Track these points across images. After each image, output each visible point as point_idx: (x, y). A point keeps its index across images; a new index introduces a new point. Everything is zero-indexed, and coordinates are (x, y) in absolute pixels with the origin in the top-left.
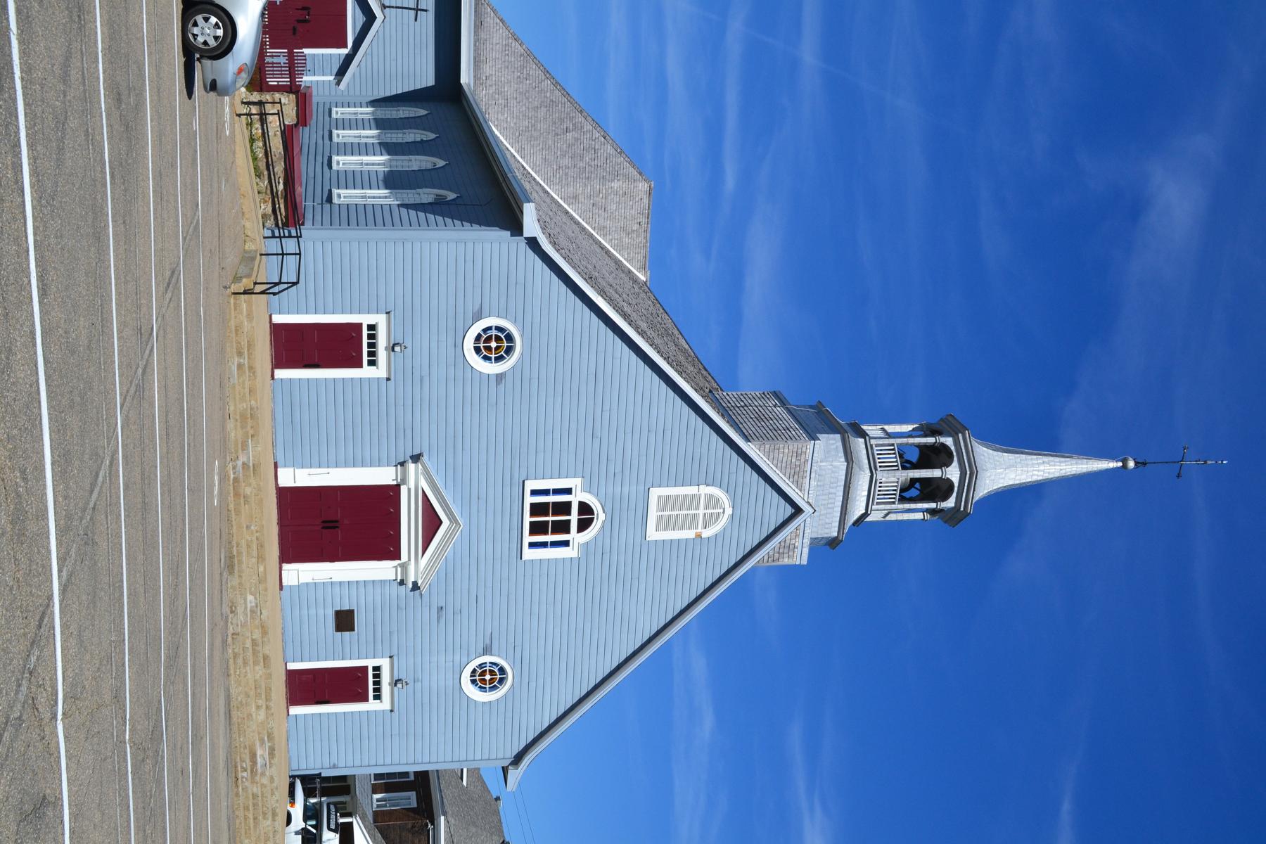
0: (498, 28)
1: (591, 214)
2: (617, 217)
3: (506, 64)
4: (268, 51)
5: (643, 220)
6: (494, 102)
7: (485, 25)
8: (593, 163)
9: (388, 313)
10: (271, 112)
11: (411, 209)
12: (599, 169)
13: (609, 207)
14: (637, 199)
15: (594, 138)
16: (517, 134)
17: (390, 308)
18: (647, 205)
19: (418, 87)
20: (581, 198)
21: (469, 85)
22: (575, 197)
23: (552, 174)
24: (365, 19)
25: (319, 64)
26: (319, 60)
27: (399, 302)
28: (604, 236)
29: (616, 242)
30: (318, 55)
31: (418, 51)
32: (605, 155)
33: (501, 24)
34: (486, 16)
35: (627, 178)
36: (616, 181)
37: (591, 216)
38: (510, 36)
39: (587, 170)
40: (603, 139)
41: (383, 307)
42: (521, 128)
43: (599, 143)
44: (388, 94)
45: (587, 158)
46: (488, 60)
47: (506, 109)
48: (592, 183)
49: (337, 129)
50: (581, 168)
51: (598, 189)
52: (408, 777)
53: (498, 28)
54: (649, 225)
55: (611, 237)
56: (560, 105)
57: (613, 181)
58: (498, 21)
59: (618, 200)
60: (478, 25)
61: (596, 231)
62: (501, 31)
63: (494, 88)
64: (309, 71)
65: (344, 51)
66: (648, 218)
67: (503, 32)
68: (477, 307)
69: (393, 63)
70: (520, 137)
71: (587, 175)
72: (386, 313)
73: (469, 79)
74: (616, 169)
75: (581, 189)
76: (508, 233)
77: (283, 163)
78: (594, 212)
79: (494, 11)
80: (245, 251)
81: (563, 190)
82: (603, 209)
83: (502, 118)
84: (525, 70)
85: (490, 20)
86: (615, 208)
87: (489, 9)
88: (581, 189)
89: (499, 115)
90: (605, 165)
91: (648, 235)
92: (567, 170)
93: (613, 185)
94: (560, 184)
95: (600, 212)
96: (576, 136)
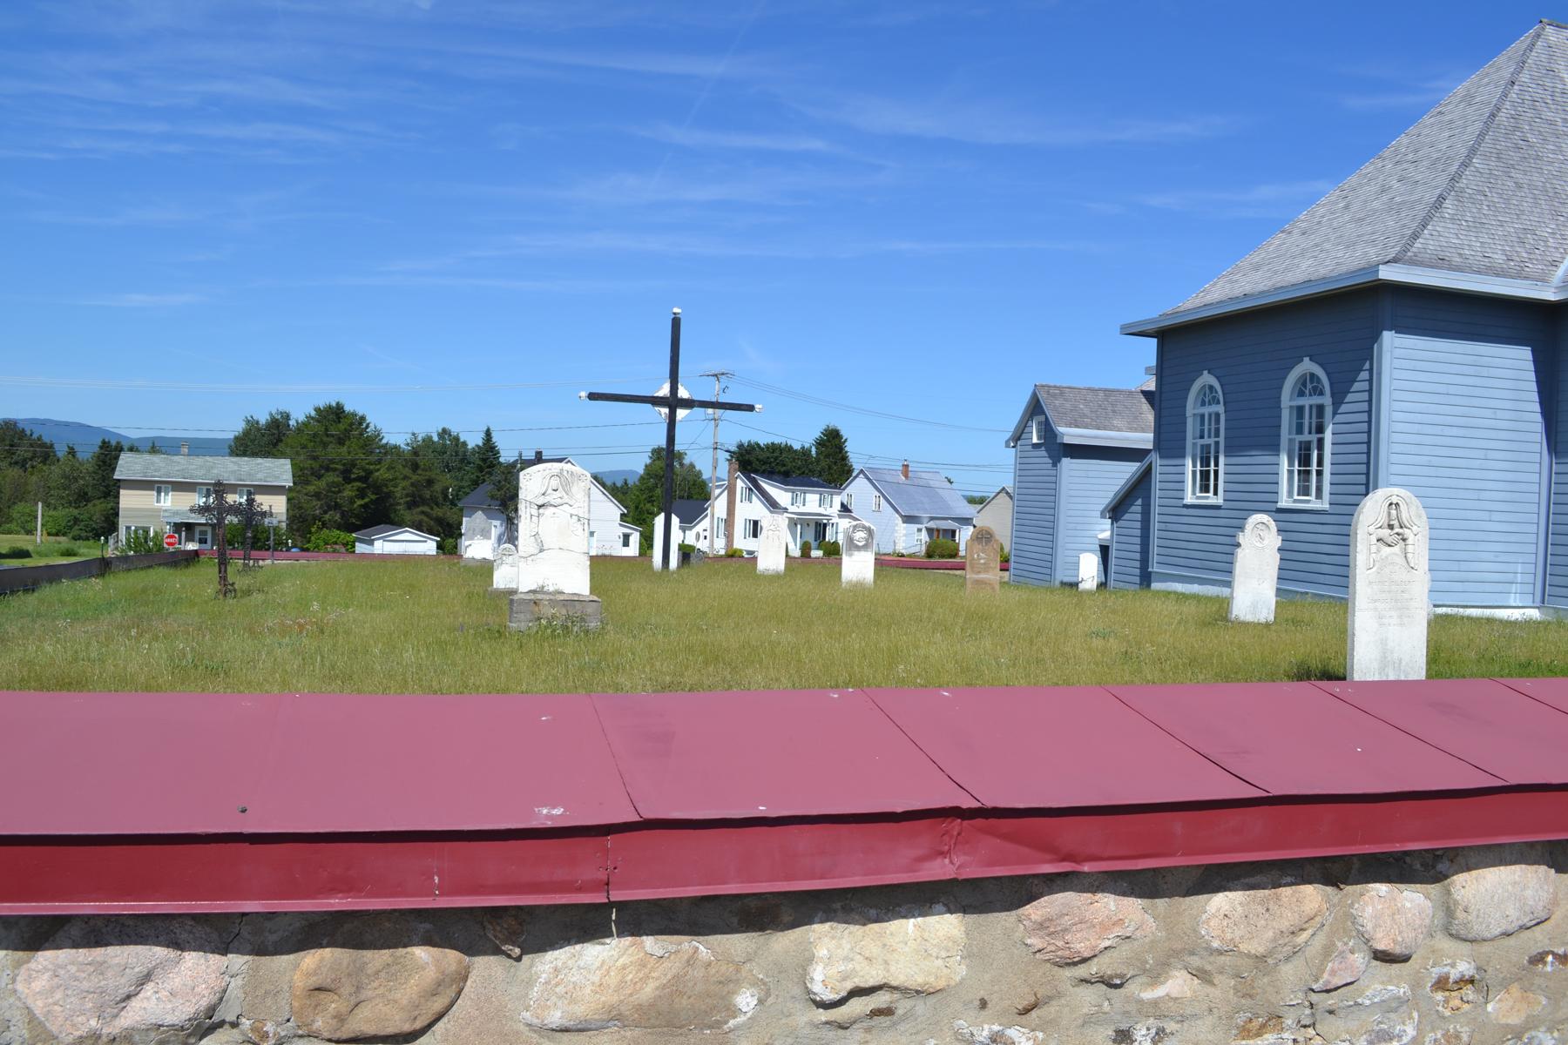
8: (1552, 106)
15: (1519, 101)
16: (1562, 219)
33: (1429, 227)
36: (1561, 75)
39: (1563, 116)
40: (1516, 87)
42: (1554, 212)
45: (1548, 114)
58: (1426, 232)
60: (1440, 263)
79: (1415, 236)
83: (1551, 240)
90: (1547, 88)
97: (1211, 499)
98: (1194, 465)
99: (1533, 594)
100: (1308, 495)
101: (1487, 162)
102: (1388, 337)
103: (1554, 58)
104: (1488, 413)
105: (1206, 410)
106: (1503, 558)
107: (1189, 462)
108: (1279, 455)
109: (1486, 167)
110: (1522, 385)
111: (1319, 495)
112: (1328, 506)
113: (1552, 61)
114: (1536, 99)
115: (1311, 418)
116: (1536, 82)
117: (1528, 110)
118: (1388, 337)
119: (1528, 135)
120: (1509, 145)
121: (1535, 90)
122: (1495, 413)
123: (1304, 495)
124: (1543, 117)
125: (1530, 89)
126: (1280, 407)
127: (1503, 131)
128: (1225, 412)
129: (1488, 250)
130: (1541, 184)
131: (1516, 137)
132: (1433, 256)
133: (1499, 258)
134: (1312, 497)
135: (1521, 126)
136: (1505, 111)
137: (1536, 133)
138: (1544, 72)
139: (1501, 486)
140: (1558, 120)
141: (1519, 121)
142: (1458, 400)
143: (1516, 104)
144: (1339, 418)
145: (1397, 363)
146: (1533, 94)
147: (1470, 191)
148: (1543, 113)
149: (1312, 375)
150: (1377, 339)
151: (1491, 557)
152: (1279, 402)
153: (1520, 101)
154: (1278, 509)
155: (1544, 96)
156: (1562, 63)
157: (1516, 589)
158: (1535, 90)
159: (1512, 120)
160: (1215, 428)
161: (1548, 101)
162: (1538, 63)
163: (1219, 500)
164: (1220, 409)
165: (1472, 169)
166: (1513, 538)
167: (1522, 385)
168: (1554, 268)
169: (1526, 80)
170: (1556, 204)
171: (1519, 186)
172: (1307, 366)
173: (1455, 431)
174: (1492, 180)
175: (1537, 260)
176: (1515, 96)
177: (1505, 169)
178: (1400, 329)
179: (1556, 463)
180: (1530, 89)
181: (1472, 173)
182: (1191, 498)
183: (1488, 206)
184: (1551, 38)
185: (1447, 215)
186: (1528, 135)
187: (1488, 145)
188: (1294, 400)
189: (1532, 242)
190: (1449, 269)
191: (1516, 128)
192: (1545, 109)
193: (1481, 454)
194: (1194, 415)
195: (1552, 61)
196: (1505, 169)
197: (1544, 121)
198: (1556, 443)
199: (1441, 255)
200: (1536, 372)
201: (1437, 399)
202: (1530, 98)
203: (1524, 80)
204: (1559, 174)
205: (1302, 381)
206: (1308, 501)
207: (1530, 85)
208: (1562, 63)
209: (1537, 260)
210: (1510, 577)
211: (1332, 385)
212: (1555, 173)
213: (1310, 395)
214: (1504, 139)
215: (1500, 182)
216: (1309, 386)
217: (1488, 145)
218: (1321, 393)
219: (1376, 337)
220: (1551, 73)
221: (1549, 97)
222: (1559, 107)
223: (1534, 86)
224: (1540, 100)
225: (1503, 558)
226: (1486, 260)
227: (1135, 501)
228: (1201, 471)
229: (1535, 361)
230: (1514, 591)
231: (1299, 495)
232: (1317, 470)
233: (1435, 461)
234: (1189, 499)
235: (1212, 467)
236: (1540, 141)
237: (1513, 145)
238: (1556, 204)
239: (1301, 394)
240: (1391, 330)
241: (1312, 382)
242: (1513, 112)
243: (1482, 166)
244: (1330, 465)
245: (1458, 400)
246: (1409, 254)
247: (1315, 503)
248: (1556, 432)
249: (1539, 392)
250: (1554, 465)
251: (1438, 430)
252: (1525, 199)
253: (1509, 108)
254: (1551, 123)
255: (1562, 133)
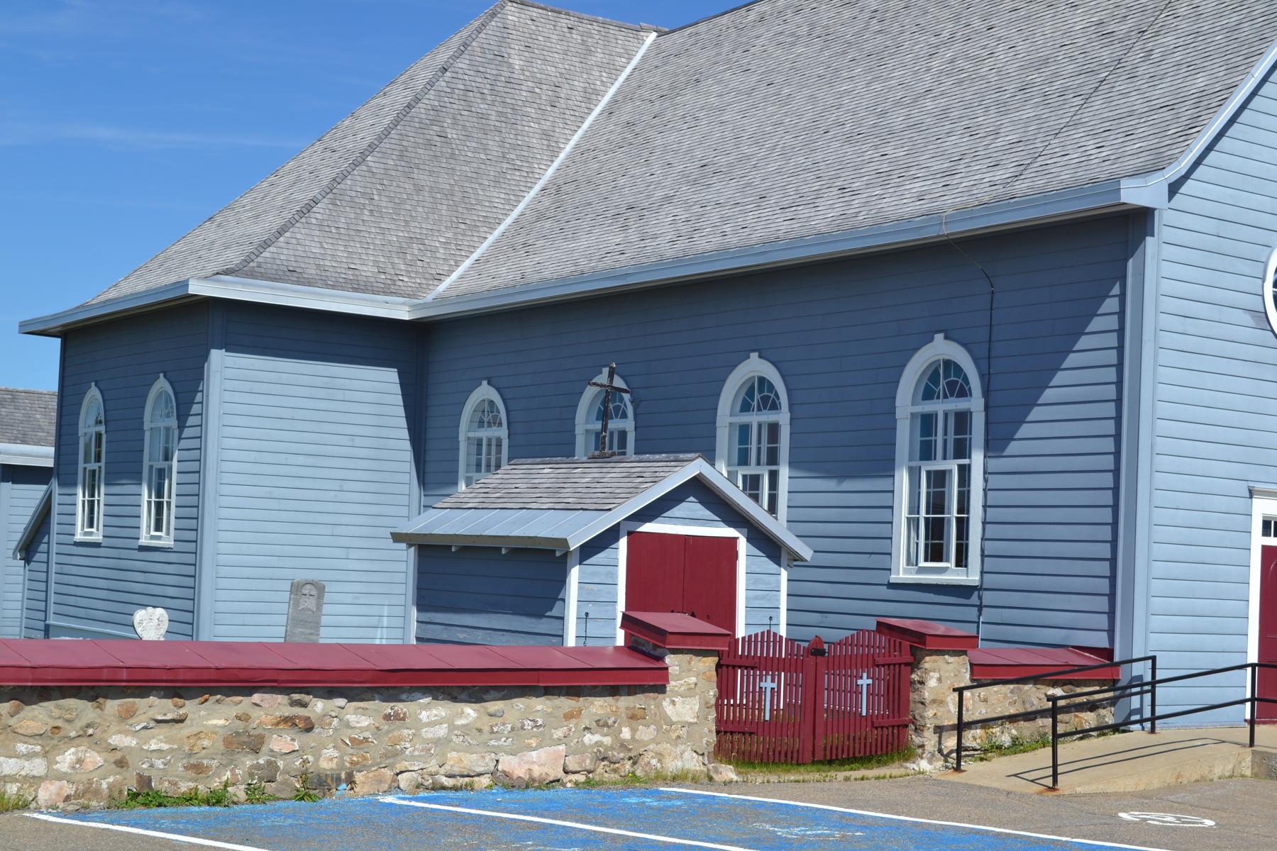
0: (294, 241)
1: (567, 112)
2: (567, 67)
3: (352, 233)
4: (738, 702)
5: (564, 22)
6: (419, 263)
7: (294, 264)
8: (489, 98)
9: (1252, 493)
10: (954, 709)
11: (186, 422)
12: (496, 88)
13: (554, 79)
14: (534, 28)
15: (449, 90)
16: (463, 226)
17: (1242, 489)
18: (540, 11)
19: (399, 400)
20: (546, 125)
21: (415, 307)
22: (546, 135)
23: (518, 173)
24: (692, 499)
25: (763, 598)
26: (756, 598)
27: (1236, 470)
28: (599, 94)
29: (604, 74)
30: (747, 599)
31: (339, 395)
32: (472, 73)
33: (287, 234)
34: (278, 262)
35: (503, 39)
36: (511, 60)
37: (572, 113)
38: (303, 220)
39: (500, 109)
40: (448, 74)
41: (1240, 504)
42: (455, 220)
43: (454, 81)
44: (408, 455)
45: (482, 106)
46: (353, 266)
47: (426, 242)
48: (520, 103)
49: (74, 535)
50: (498, 119)
51: (528, 94)
52: (165, 469)
53: (294, 241)
54: (571, 13)
55: (598, 83)
56: (405, 143)
57: (510, 66)
58: (282, 239)
59: (539, 62)
60: (291, 275)
61: (592, 106)
62: (298, 236)
63: (396, 261)
64: (771, 618)
65: (743, 546)
66: (559, 13)
67: (299, 232)
68: (1247, 319)
69: (358, 441)
70: (468, 222)
71: (509, 111)
72: (1251, 497)
73: (404, 304)
74: (492, 57)
75: (532, 124)
76: (1148, 239)
77: (1026, 687)
78: (564, 106)
79: (266, 244)
80: (1255, 775)
81: (538, 156)
82: (557, 89)
83: (442, 251)
84: (357, 200)
85: (281, 253)
86: (553, 69)
87: (266, 254)
88: (532, 124)
89: (438, 255)
90: (488, 76)
91: (585, 16)
92: (507, 145)
93: (517, 67)
94: (530, 160)
95: (562, 95)
96: (449, 121)
97: (950, 574)
98: (150, 496)
99: (287, 626)
100: (941, 560)
101: (384, 161)
102: (217, 356)
103: (508, 40)
104: (344, 440)
105: (484, 434)
106: (363, 599)
107: (80, 491)
108: (141, 484)
109: (382, 166)
110: (386, 410)
111: (962, 561)
112: (173, 543)
113: (504, 45)
114: (470, 88)
115: (945, 433)
116: (475, 68)
117: (456, 102)
118: (217, 356)
119: (448, 130)
120: (421, 141)
121: (471, 78)
122: (353, 440)
123: (932, 560)
124: (473, 109)
125: (466, 77)
126: (143, 429)
127: (417, 125)
128: (636, 428)
129: (357, 261)
130: (448, 187)
131: (431, 132)
132: (282, 268)
133: (368, 270)
134: (951, 564)
135: (441, 119)
136: (427, 102)
137: (460, 127)
138: (492, 57)
139: (361, 520)
140: (493, 113)
141: (440, 114)
142: (308, 426)
143: (442, 94)
144: (184, 444)
145: (229, 385)
146: (468, 83)
147: (354, 194)
148: (476, 105)
149: (762, 380)
150: (207, 358)
151: (349, 598)
152: (142, 423)
153: (449, 90)
154: (140, 546)
155: (482, 85)
156: (517, 47)
157: (382, 633)
158: (471, 78)
159: (432, 112)
160: (769, 449)
161: (485, 91)
162: (485, 46)
163: (970, 576)
164: (503, 432)
165: (364, 168)
166: (376, 577)
167: (386, 410)
168: (436, 283)
169: (464, 66)
170: (461, 210)
171: (418, 189)
172: (755, 366)
173: (301, 460)
174: (385, 182)
175: (416, 272)
176: (443, 84)
177: (406, 169)
178: (231, 346)
179: (424, 495)
180: (466, 77)
181: (363, 173)
182: (905, 571)
183: (371, 211)
184: (510, 17)
185: (314, 221)
186: (448, 130)
187: (393, 141)
188: (736, 415)
189: (416, 252)
190: (298, 283)
191: (434, 122)
192: (479, 101)
193: (335, 485)
194: (587, 431)
195: (504, 45)
196: (406, 169)
197: (475, 114)
198: (424, 473)
199: (293, 265)
200: (403, 395)
201: (278, 424)
202: (462, 87)
203: (460, 65)
204: (475, 175)
205: (745, 390)
206: (159, 538)
207: (468, 72)
208: (517, 47)
209: (416, 272)
210: (374, 621)
211: (789, 391)
212: (469, 175)
213: (759, 409)
214: (413, 134)
215: (395, 184)
216: (757, 396)
217: (393, 141)
218: (775, 407)
219: (206, 357)
220: (499, 58)
221: (488, 86)
222: (498, 99)
223: (472, 73)
224: (475, 90)
225: (363, 599)
226: (350, 272)
227: (43, 539)
228: (927, 520)
229: (402, 384)
230: (379, 636)
231: (926, 560)
232: (958, 519)
233: (277, 493)
234: (902, 573)
235: (96, 497)
236: (461, 137)
237: (426, 142)
238: (461, 210)
239: (746, 407)
240: (221, 349)
241: (761, 390)
242: (436, 103)
243: (377, 165)
244: (175, 496)
245: (308, 426)
246: (252, 264)
247: (953, 572)
248: (425, 462)
249: (407, 417)
250: (422, 496)
251: (281, 458)
252: (421, 204)
253: (432, 97)
254: (483, 116)
255: (492, 128)
